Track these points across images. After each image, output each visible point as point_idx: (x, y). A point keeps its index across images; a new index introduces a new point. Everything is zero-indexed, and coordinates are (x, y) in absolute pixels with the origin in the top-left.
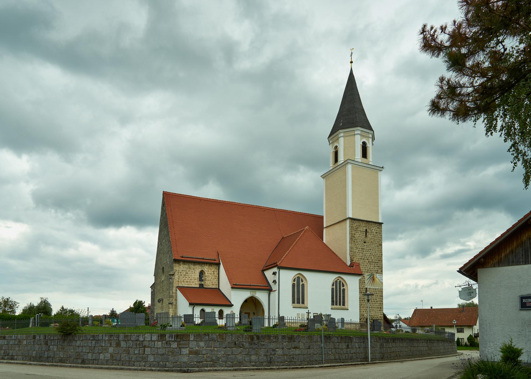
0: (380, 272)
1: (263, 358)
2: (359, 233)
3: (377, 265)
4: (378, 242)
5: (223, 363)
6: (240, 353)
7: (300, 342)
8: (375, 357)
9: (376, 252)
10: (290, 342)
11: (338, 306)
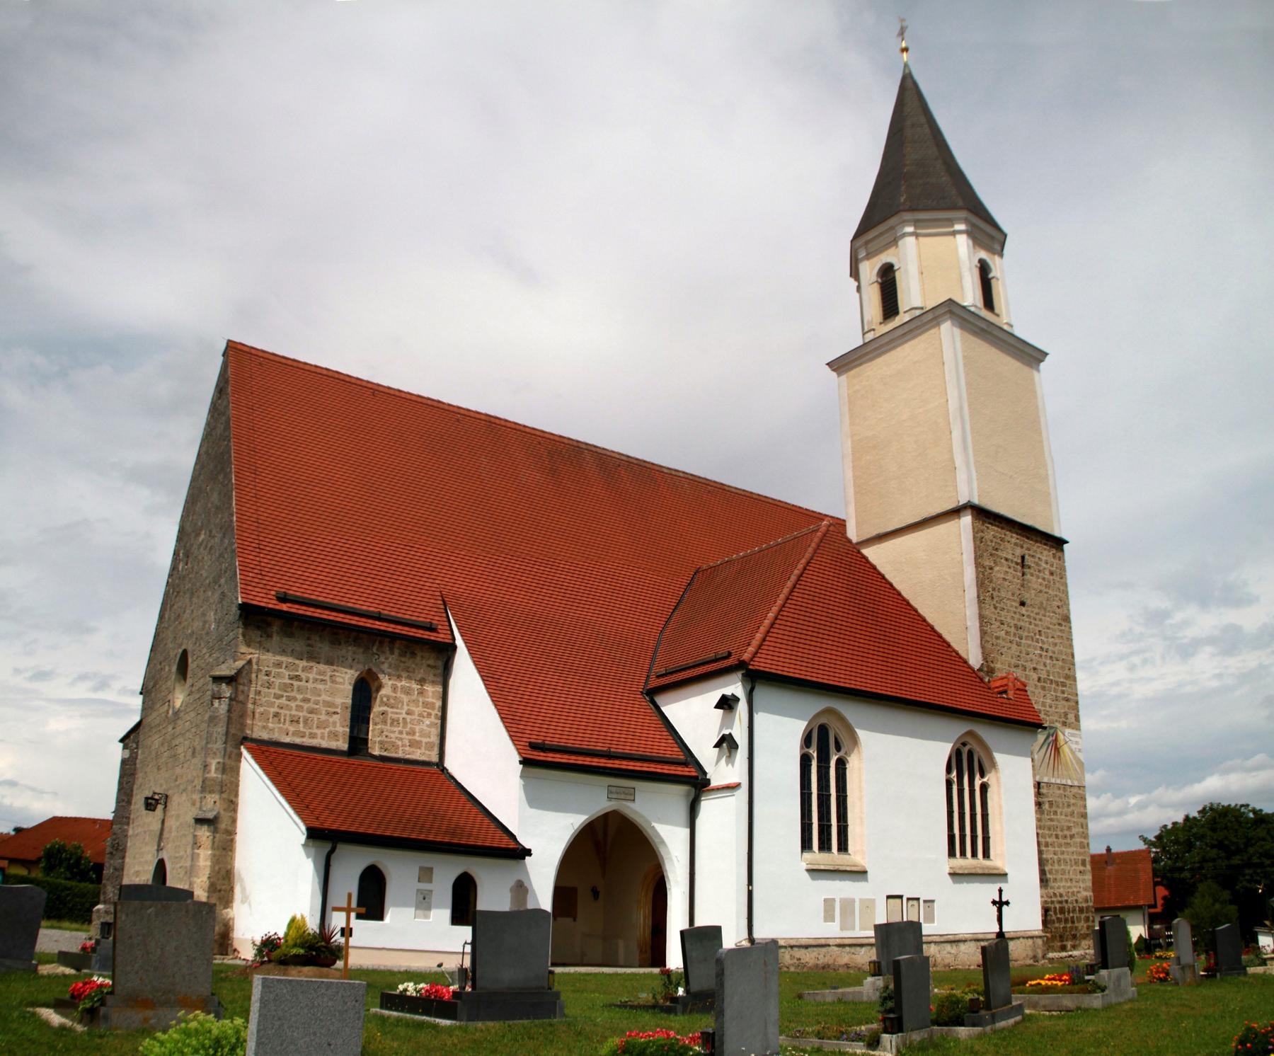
0: (1073, 720)
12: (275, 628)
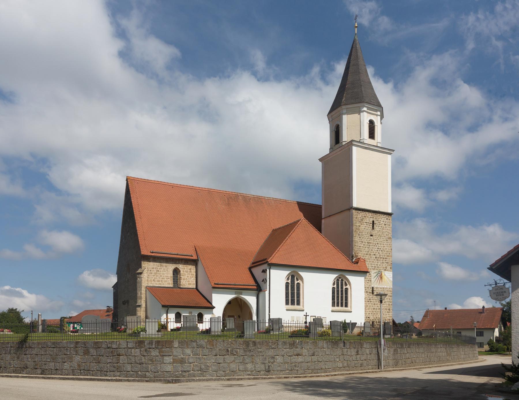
1: (260, 367)
2: (364, 225)
3: (386, 261)
4: (387, 235)
5: (214, 372)
6: (234, 361)
7: (304, 348)
8: (388, 364)
9: (384, 246)
10: (292, 348)
11: (340, 308)
12: (151, 260)
